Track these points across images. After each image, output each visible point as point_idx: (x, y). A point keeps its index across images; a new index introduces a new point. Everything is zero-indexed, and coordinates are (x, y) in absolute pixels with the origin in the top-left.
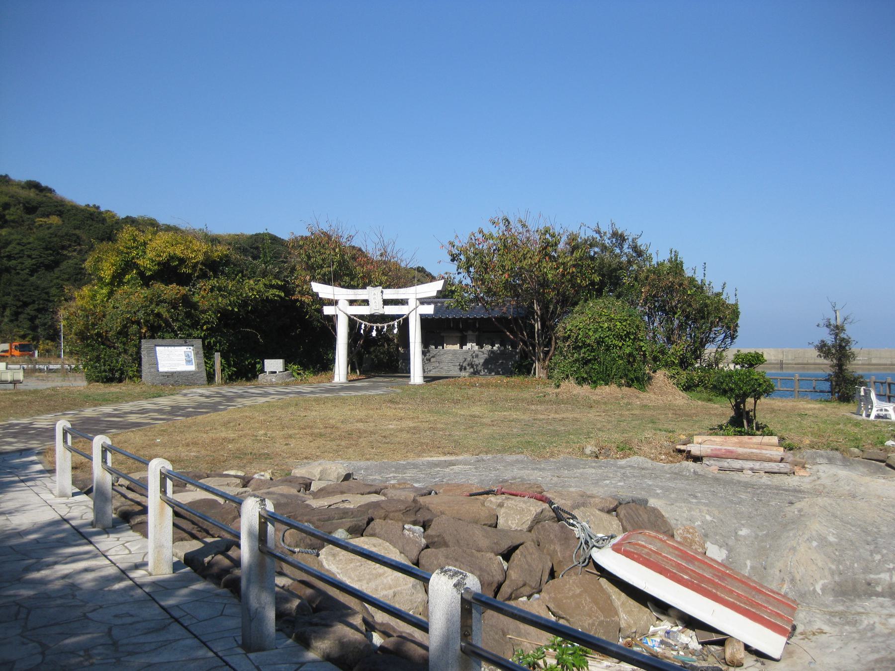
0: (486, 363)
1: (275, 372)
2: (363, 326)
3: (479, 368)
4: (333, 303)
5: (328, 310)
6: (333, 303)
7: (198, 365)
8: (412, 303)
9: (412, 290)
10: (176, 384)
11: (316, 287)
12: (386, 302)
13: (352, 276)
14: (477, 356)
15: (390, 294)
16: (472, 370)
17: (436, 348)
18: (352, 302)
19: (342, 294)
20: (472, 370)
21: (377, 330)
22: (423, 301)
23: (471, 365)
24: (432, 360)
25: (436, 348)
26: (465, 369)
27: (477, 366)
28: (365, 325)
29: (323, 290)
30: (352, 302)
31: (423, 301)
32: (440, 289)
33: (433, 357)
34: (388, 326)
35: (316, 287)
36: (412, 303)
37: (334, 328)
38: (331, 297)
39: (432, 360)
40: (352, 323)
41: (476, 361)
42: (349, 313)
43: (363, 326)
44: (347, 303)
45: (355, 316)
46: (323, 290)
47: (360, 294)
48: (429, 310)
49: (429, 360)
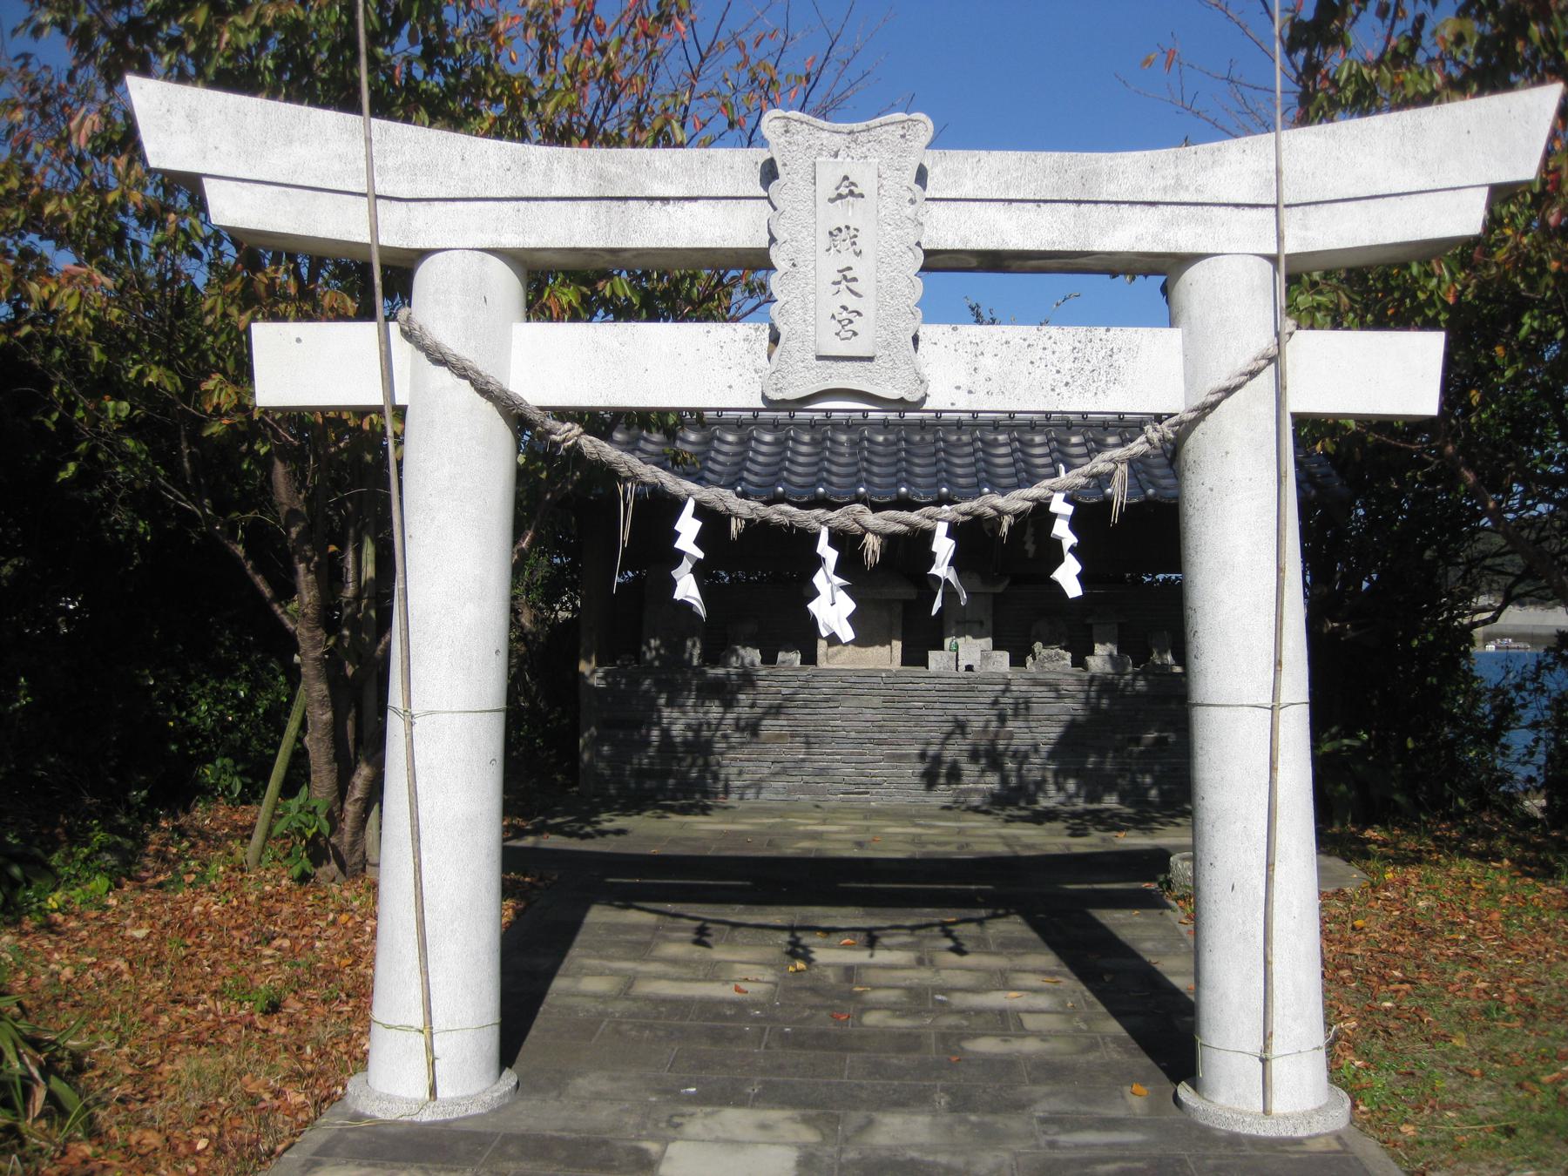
0: (1073, 746)
2: (688, 528)
3: (1036, 768)
4: (369, 283)
5: (303, 365)
6: (369, 283)
8: (1235, 301)
9: (1237, 165)
10: (498, 398)
11: (180, 123)
12: (970, 277)
13: (316, 305)
14: (1023, 707)
15: (1002, 197)
16: (992, 782)
17: (769, 659)
18: (565, 286)
19: (462, 199)
20: (992, 782)
22: (1363, 290)
23: (991, 758)
24: (769, 726)
25: (769, 659)
26: (954, 775)
27: (1021, 758)
28: (711, 518)
29: (253, 157)
30: (565, 286)
31: (1363, 290)
32: (1526, 168)
33: (776, 711)
34: (969, 534)
37: (392, 543)
38: (340, 223)
39: (769, 726)
40: (571, 498)
41: (1020, 734)
43: (688, 528)
44: (506, 285)
46: (253, 157)
47: (681, 199)
48: (1395, 374)
49: (753, 728)
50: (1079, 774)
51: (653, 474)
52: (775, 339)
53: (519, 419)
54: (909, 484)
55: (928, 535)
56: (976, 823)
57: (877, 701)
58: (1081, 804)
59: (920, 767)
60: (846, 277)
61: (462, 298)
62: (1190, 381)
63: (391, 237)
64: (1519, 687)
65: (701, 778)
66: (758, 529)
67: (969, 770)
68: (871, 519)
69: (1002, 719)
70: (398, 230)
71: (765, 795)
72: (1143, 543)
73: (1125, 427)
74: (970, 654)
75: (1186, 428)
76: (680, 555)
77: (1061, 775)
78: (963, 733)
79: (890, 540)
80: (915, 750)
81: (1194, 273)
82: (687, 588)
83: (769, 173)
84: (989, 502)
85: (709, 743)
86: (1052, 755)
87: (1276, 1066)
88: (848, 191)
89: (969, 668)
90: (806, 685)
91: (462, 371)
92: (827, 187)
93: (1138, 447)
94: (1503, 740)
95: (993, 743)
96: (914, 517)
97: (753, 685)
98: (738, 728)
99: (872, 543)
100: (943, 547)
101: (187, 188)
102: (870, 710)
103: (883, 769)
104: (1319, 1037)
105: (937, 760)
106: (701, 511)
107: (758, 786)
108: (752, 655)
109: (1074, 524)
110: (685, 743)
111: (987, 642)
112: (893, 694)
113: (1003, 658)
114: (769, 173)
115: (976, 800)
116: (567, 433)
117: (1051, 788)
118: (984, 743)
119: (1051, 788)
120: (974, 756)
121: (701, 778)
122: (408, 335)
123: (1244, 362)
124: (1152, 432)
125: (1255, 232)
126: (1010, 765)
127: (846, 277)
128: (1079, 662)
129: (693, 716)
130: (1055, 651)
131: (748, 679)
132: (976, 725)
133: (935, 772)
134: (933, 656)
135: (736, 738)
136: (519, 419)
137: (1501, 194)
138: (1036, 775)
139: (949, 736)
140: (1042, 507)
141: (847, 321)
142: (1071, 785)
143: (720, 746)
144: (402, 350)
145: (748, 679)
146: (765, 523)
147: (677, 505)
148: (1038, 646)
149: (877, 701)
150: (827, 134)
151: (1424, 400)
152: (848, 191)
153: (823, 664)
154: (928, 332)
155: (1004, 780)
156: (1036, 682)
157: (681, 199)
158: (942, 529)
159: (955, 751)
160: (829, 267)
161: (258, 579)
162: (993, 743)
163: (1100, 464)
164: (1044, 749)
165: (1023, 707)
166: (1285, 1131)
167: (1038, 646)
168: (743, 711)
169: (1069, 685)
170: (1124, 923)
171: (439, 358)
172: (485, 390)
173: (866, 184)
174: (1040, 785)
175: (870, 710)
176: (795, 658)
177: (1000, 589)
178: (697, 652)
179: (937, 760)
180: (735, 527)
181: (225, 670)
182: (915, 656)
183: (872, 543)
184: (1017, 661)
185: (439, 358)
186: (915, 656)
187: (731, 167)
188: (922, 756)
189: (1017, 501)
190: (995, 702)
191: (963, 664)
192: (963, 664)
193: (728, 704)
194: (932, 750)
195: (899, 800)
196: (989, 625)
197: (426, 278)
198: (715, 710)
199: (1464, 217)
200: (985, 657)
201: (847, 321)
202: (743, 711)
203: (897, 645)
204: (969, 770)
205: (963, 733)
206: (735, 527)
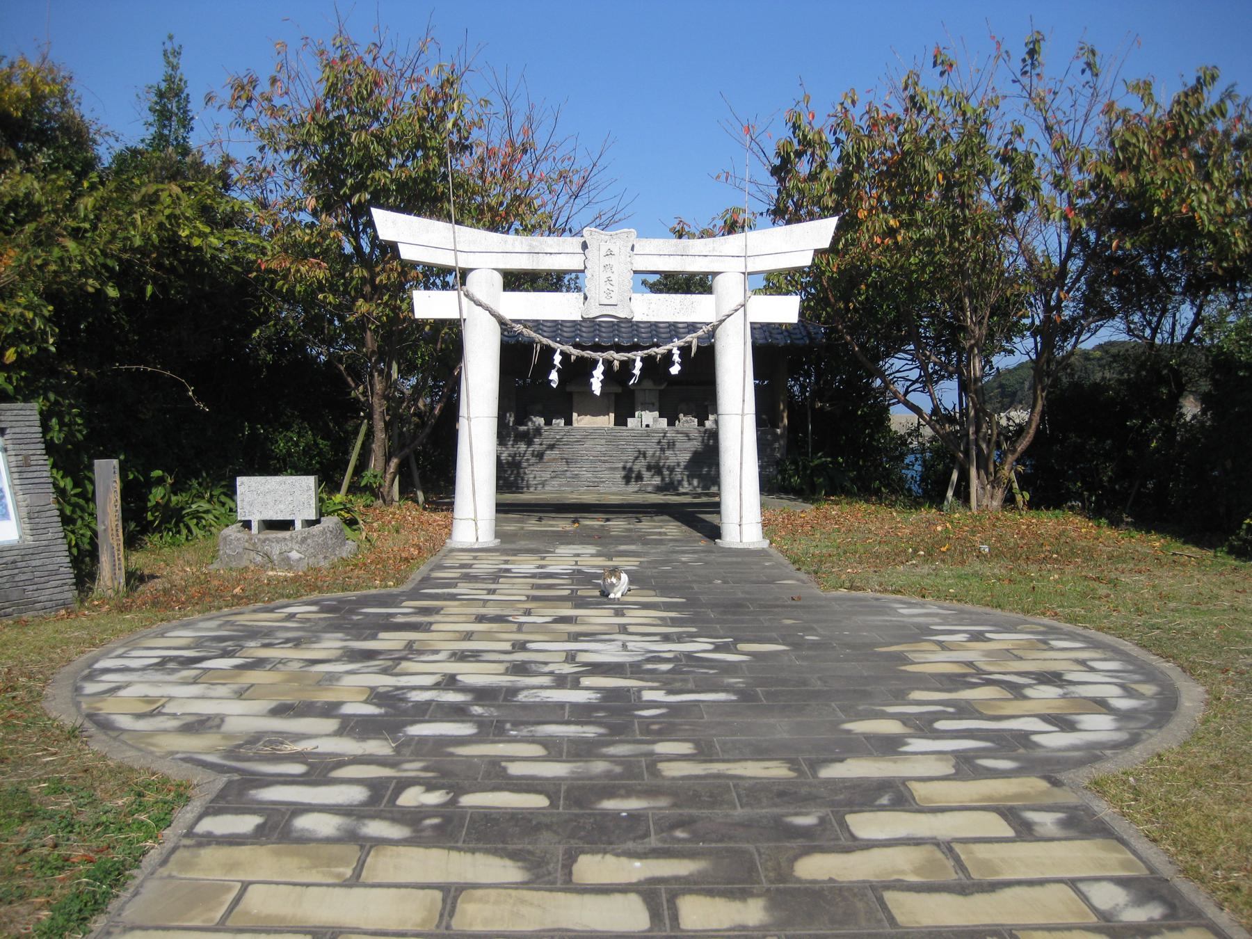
1: (286, 525)
2: (557, 358)
5: (429, 305)
7: (32, 517)
11: (390, 224)
14: (672, 445)
16: (657, 481)
17: (548, 423)
18: (515, 280)
19: (484, 251)
20: (657, 481)
21: (608, 372)
22: (776, 283)
23: (656, 469)
25: (548, 423)
26: (639, 477)
27: (671, 469)
30: (515, 280)
31: (776, 283)
33: (551, 447)
34: (647, 360)
35: (390, 224)
36: (730, 288)
38: (446, 260)
41: (671, 458)
42: (509, 315)
43: (557, 358)
44: (498, 280)
45: (524, 323)
47: (553, 253)
48: (785, 310)
49: (540, 456)
50: (700, 477)
51: (545, 341)
52: (586, 298)
53: (502, 323)
54: (619, 337)
55: (634, 361)
56: (653, 496)
57: (603, 442)
58: (699, 490)
59: (623, 473)
60: (609, 280)
61: (485, 284)
62: (717, 313)
63: (462, 264)
64: (910, 435)
65: (516, 480)
66: (580, 359)
67: (646, 475)
68: (616, 356)
69: (662, 450)
70: (463, 263)
71: (547, 488)
72: (702, 362)
73: (692, 327)
74: (648, 418)
75: (715, 328)
76: (554, 366)
77: (690, 477)
78: (645, 457)
79: (622, 362)
80: (621, 465)
81: (718, 278)
82: (554, 376)
83: (585, 246)
84: (653, 351)
85: (520, 462)
86: (686, 468)
87: (744, 527)
88: (610, 254)
89: (647, 426)
90: (568, 434)
91: (487, 308)
92: (604, 251)
93: (700, 333)
94: (275, 193)
95: (658, 463)
96: (629, 355)
97: (540, 434)
98: (533, 455)
99: (616, 363)
100: (639, 365)
101: (392, 247)
102: (600, 447)
103: (606, 475)
104: (759, 519)
105: (631, 470)
106: (562, 353)
107: (543, 484)
108: (540, 421)
109: (680, 356)
110: (508, 463)
111: (656, 414)
112: (611, 439)
113: (664, 422)
114: (585, 246)
115: (650, 489)
116: (519, 327)
117: (685, 484)
118: (653, 463)
119: (685, 484)
120: (649, 468)
121: (516, 480)
122: (467, 295)
123: (734, 307)
124: (705, 329)
125: (739, 265)
126: (666, 473)
127: (609, 280)
128: (701, 424)
129: (512, 450)
130: (689, 418)
131: (538, 431)
132: (650, 453)
133: (630, 476)
134: (629, 420)
135: (533, 460)
136: (502, 323)
137: (818, 252)
138: (679, 477)
139: (637, 458)
140: (670, 351)
141: (609, 293)
142: (695, 482)
143: (524, 464)
144: (464, 300)
145: (538, 431)
146: (582, 357)
147: (553, 351)
148: (681, 416)
149: (603, 442)
150: (602, 235)
151: (794, 319)
152: (610, 254)
153: (575, 424)
154: (634, 296)
155: (663, 479)
156: (678, 432)
157: (553, 253)
158: (638, 359)
159: (640, 466)
160: (604, 277)
161: (349, 379)
162: (658, 463)
163: (688, 338)
164: (682, 464)
165: (672, 445)
166: (746, 546)
167: (681, 416)
168: (536, 447)
169: (695, 434)
170: (708, 517)
171: (479, 304)
172: (493, 314)
173: (615, 251)
174: (680, 482)
175: (600, 447)
176: (562, 422)
177: (662, 387)
178: (512, 419)
179: (631, 470)
180: (573, 358)
181: (288, 427)
182: (621, 421)
183: (616, 363)
184: (671, 423)
185: (479, 304)
186: (621, 421)
187: (573, 243)
188: (624, 468)
189: (662, 350)
190: (659, 442)
191: (644, 424)
192: (644, 424)
193: (530, 443)
194: (629, 465)
195: (614, 489)
196: (657, 405)
197: (471, 278)
198: (522, 447)
199: (805, 260)
200: (655, 421)
201: (609, 293)
202: (536, 447)
203: (612, 415)
204: (646, 475)
205: (645, 457)
206: (573, 358)
